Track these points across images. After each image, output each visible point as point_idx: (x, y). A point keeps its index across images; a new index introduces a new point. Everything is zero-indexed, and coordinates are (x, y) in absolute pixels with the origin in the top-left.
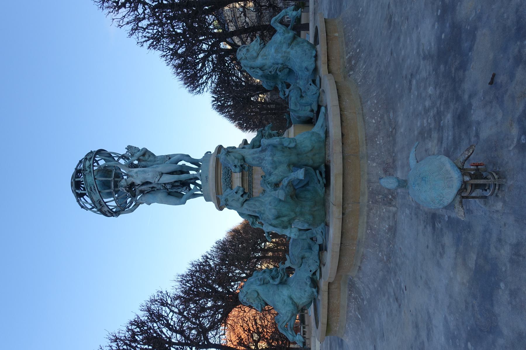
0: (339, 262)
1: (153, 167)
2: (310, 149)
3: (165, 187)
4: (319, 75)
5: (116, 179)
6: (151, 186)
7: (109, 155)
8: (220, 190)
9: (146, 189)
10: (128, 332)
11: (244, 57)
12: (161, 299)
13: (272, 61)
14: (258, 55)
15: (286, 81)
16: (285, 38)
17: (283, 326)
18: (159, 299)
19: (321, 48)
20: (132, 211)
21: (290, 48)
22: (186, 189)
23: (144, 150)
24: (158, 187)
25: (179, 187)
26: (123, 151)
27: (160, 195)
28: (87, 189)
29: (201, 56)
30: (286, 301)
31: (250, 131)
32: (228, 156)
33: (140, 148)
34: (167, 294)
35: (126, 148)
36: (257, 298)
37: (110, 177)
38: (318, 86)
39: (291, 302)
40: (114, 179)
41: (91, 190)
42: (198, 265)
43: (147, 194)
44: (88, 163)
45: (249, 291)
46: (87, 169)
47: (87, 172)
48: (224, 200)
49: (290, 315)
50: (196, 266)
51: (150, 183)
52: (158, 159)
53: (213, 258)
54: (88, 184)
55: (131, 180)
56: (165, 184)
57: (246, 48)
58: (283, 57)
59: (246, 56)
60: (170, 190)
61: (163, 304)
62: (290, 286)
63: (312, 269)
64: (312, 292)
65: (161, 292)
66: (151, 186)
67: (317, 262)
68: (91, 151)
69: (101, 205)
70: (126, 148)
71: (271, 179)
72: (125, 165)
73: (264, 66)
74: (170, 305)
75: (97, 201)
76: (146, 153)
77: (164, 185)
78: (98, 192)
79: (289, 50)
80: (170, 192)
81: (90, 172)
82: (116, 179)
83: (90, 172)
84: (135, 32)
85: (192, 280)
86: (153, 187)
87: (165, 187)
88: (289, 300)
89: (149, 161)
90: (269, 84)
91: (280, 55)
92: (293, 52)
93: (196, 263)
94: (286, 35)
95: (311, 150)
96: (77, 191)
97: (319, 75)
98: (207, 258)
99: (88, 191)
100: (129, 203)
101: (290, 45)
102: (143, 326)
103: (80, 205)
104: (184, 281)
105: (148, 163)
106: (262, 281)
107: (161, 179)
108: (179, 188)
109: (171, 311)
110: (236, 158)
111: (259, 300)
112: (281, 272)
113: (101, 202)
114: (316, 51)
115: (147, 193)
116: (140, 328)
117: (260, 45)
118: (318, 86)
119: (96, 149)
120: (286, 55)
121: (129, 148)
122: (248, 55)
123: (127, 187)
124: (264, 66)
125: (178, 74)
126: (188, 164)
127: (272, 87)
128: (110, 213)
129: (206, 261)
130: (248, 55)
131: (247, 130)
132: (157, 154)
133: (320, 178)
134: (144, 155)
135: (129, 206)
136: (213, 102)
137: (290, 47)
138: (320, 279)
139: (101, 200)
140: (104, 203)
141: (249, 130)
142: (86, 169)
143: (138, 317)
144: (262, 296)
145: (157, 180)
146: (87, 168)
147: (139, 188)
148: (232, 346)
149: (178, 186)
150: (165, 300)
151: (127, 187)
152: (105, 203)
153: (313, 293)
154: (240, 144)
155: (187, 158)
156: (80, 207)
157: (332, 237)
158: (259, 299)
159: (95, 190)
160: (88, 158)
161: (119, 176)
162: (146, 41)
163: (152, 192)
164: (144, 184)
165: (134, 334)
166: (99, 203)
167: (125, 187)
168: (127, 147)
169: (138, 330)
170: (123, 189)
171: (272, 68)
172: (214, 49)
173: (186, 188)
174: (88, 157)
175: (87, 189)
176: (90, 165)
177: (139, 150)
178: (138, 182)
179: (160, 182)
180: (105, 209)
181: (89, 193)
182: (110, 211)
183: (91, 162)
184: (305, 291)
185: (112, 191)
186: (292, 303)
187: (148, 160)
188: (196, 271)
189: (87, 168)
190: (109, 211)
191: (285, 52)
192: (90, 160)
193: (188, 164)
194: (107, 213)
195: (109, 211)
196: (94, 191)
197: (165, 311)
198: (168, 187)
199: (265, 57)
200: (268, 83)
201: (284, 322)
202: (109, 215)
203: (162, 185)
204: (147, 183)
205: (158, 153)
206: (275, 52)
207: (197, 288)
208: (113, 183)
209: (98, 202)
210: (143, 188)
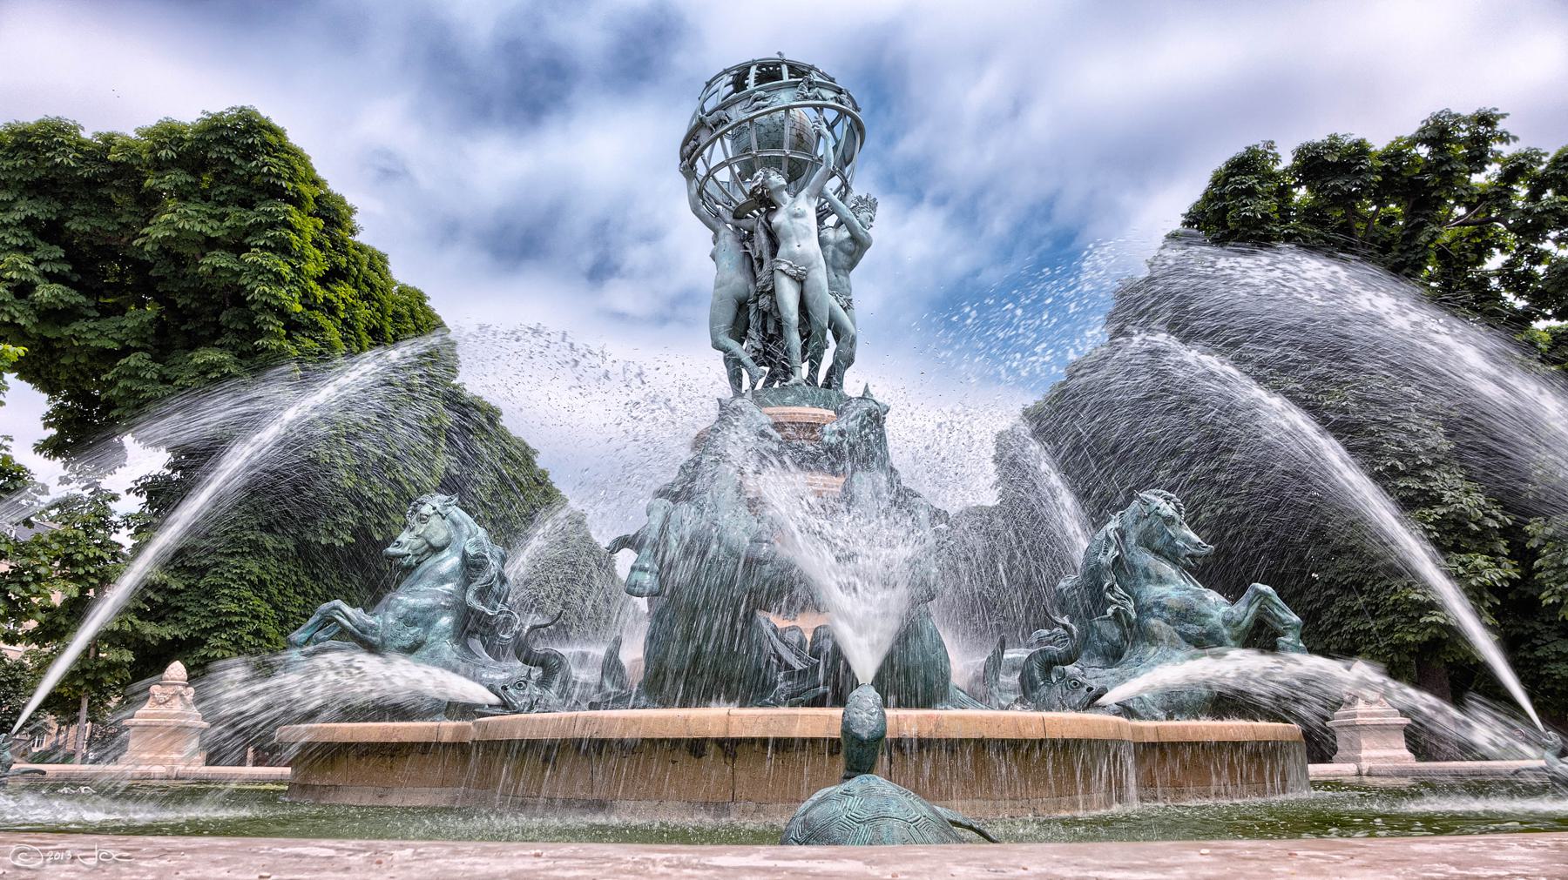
6: (766, 256)
7: (847, 158)
9: (756, 244)
24: (763, 275)
40: (787, 156)
41: (756, 100)
51: (774, 254)
52: (841, 277)
56: (772, 292)
60: (753, 307)
66: (766, 256)
69: (715, 126)
77: (769, 289)
78: (752, 115)
81: (806, 98)
86: (761, 261)
96: (753, 70)
99: (753, 92)
106: (255, 395)
111: (419, 552)
126: (827, 361)
128: (693, 150)
145: (784, 267)
149: (765, 329)
157: (150, 816)
159: (758, 109)
163: (747, 262)
167: (763, 186)
174: (843, 97)
176: (824, 99)
178: (779, 219)
179: (777, 274)
180: (704, 137)
190: (696, 147)
193: (827, 361)
194: (692, 143)
195: (696, 147)
198: (764, 302)
204: (774, 246)
209: (723, 117)
210: (761, 238)
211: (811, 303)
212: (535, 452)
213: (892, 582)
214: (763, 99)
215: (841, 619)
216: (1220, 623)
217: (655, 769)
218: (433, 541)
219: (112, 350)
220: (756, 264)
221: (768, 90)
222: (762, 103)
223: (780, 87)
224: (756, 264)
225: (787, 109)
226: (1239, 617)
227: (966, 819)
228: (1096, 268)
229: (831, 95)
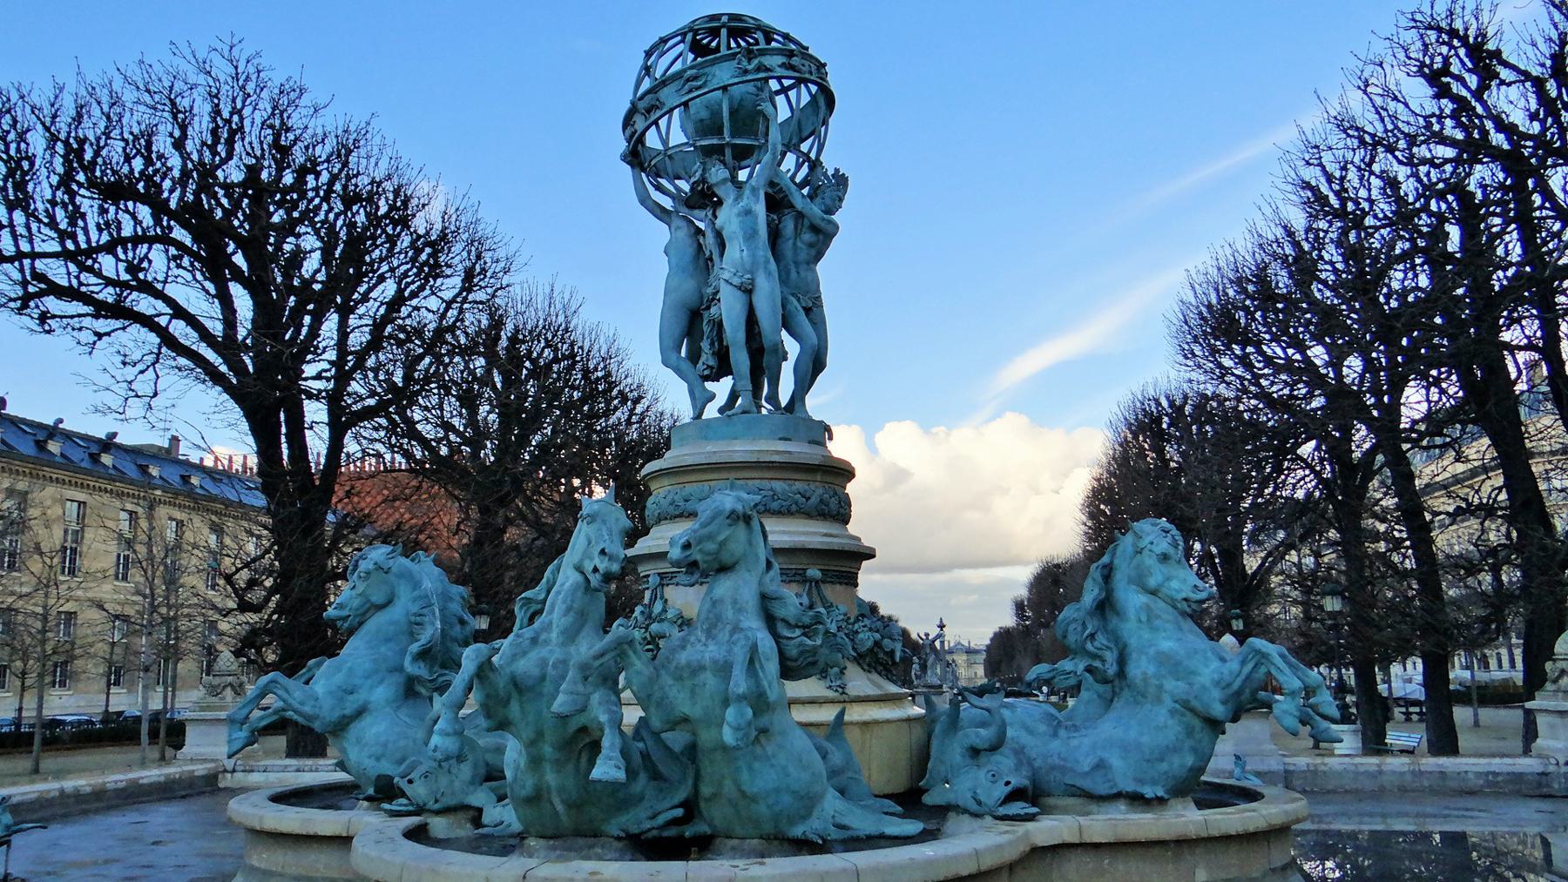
1: (767, 262)
2: (744, 788)
4: (1038, 814)
5: (728, 152)
6: (716, 257)
8: (693, 478)
10: (372, 183)
11: (1142, 544)
12: (484, 271)
13: (1133, 642)
14: (1154, 593)
16: (1204, 687)
18: (485, 263)
19: (1187, 818)
20: (645, 200)
21: (1173, 705)
22: (708, 367)
23: (830, 228)
29: (1318, 354)
30: (351, 697)
31: (1090, 528)
32: (728, 521)
35: (837, 170)
37: (733, 136)
38: (1001, 809)
39: (347, 712)
41: (688, 80)
42: (608, 374)
45: (391, 577)
46: (755, 62)
50: (605, 367)
51: (722, 255)
52: (803, 274)
53: (634, 419)
54: (706, 70)
55: (726, 193)
57: (1171, 551)
58: (1145, 680)
59: (1146, 552)
60: (706, 314)
61: (469, 275)
62: (398, 708)
63: (415, 784)
65: (506, 271)
67: (436, 801)
68: (824, 65)
70: (837, 170)
71: (637, 662)
72: (777, 173)
73: (1118, 614)
74: (465, 299)
76: (823, 235)
79: (1169, 703)
80: (701, 315)
81: (746, 72)
82: (728, 152)
84: (1348, 135)
85: (556, 360)
88: (355, 706)
89: (794, 244)
90: (1071, 628)
91: (1151, 670)
92: (1161, 715)
94: (1216, 694)
95: (743, 793)
97: (1038, 814)
98: (637, 401)
100: (676, 187)
101: (1187, 706)
102: (395, 223)
103: (664, 41)
104: (550, 336)
105: (791, 242)
107: (729, 287)
108: (712, 344)
110: (722, 544)
114: (1161, 801)
116: (386, 216)
118: (1002, 811)
119: (833, 83)
120: (1152, 690)
121: (841, 181)
122: (1150, 557)
124: (1118, 614)
125: (1239, 282)
127: (1065, 637)
129: (624, 399)
130: (1149, 561)
131: (1092, 516)
132: (821, 268)
133: (661, 820)
134: (815, 229)
135: (659, 188)
136: (1167, 398)
137: (1178, 706)
138: (386, 811)
141: (1089, 524)
142: (756, 57)
143: (424, 206)
144: (375, 622)
148: (334, 500)
150: (481, 283)
152: (656, 123)
154: (859, 539)
155: (814, 365)
158: (367, 612)
159: (690, 91)
161: (743, 155)
162: (1329, 178)
164: (719, 235)
165: (371, 199)
169: (383, 210)
170: (698, 175)
171: (1105, 642)
172: (1344, 402)
176: (768, 70)
177: (830, 211)
180: (640, 123)
183: (780, 72)
184: (378, 759)
186: (344, 716)
191: (1160, 687)
192: (787, 69)
197: (450, 285)
199: (1144, 618)
202: (628, 132)
205: (831, 272)
206: (1158, 653)
207: (533, 374)
208: (715, 141)
211: (756, 322)
212: (624, 158)
213: (821, 664)
214: (695, 78)
215: (214, 337)
216: (1208, 684)
222: (694, 83)
225: (725, 88)
226: (1227, 678)
228: (433, 497)
229: (780, 60)
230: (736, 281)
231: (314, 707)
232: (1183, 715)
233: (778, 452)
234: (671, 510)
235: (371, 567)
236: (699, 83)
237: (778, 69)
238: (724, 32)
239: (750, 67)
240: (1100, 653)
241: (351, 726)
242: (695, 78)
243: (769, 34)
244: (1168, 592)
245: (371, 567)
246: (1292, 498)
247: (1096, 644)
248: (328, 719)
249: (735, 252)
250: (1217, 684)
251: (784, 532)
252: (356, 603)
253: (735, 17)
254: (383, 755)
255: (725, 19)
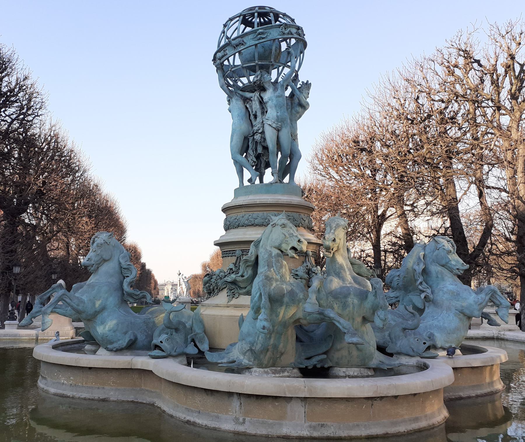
0: (188, 386)
3: (256, 132)
6: (259, 114)
15: (400, 303)
17: (65, 297)
24: (257, 124)
25: (255, 152)
26: (302, 78)
27: (244, 127)
28: (260, 29)
33: (308, 100)
34: (38, 116)
35: (308, 81)
36: (102, 259)
40: (257, 64)
41: (259, 34)
43: (244, 110)
44: (294, 31)
47: (284, 30)
48: (284, 223)
49: (80, 308)
54: (267, 31)
57: (452, 250)
60: (251, 139)
64: (112, 341)
65: (40, 108)
66: (259, 114)
69: (237, 46)
70: (308, 81)
75: (243, 41)
76: (304, 107)
77: (260, 131)
83: (284, 34)
86: (255, 116)
87: (256, 132)
93: (72, 155)
99: (258, 30)
103: (231, 20)
107: (271, 128)
108: (253, 151)
109: (13, 120)
111: (97, 263)
112: (141, 295)
113: (241, 46)
115: (247, 108)
117: (458, 269)
121: (307, 85)
123: (260, 82)
128: (223, 57)
139: (245, 47)
140: (240, 50)
146: (289, 30)
147: (256, 97)
149: (256, 150)
151: (260, 82)
153: (111, 342)
156: (212, 58)
159: (260, 39)
160: (300, 30)
164: (262, 102)
166: (240, 43)
168: (309, 83)
173: (255, 162)
175: (260, 29)
181: (255, 32)
182: (226, 57)
185: (257, 62)
187: (293, 111)
188: (61, 156)
189: (289, 30)
192: (297, 34)
195: (225, 55)
196: (259, 36)
200: (397, 278)
201: (71, 300)
203: (260, 129)
209: (241, 42)
214: (262, 33)
217: (252, 398)
218: (104, 257)
219: (83, 340)
220: (252, 117)
221: (265, 29)
223: (272, 27)
224: (252, 117)
226: (480, 301)
227: (261, 253)
230: (274, 125)
231: (83, 306)
232: (459, 315)
233: (285, 199)
234: (246, 222)
235: (102, 241)
236: (264, 36)
237: (295, 34)
238: (256, 14)
239: (286, 32)
240: (425, 290)
241: (98, 316)
242: (262, 33)
243: (277, 16)
244: (450, 266)
245: (102, 241)
246: (25, 211)
247: (423, 286)
248: (89, 313)
249: (272, 113)
250: (476, 303)
251: (255, 234)
252: (97, 259)
253: (260, 8)
254: (117, 330)
255: (257, 8)
